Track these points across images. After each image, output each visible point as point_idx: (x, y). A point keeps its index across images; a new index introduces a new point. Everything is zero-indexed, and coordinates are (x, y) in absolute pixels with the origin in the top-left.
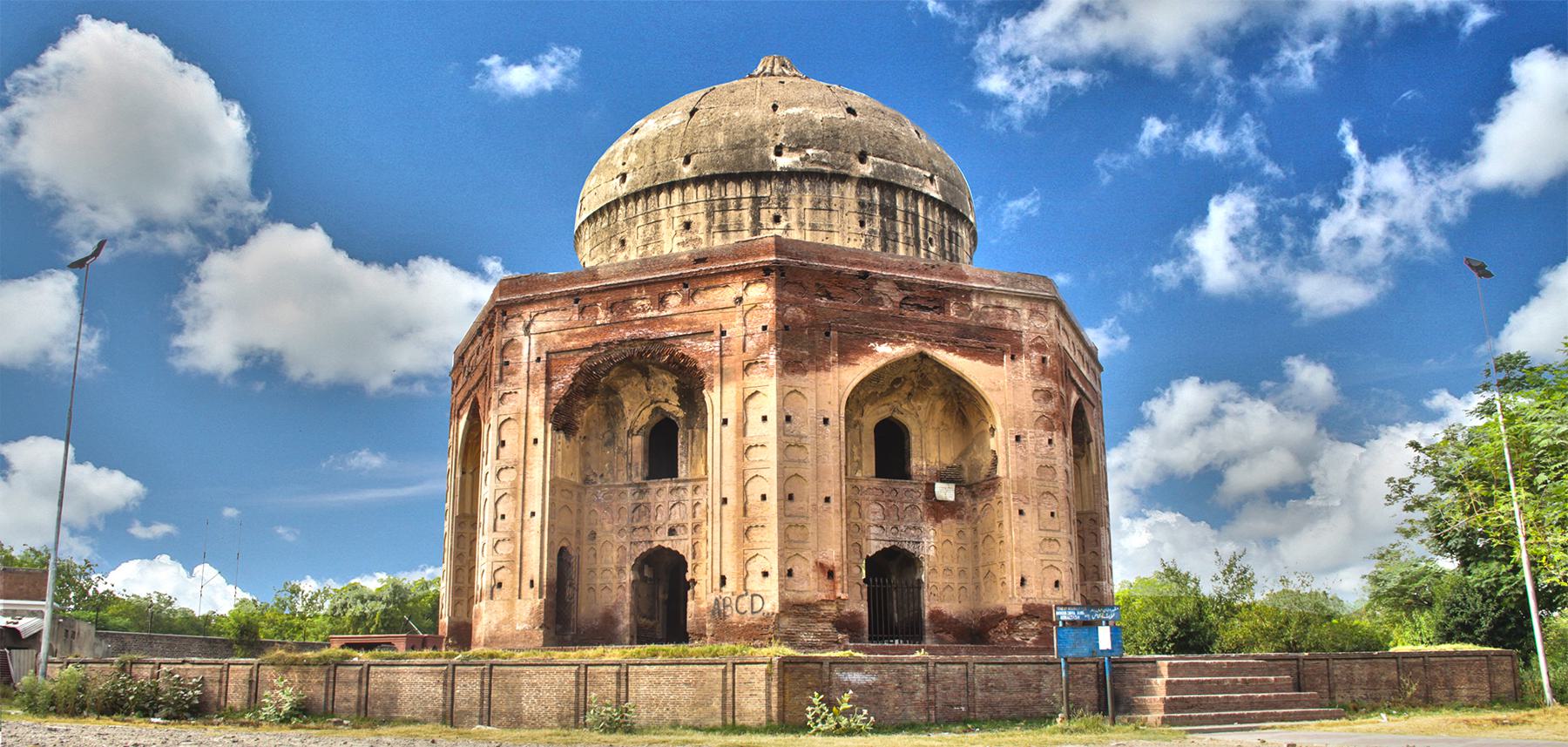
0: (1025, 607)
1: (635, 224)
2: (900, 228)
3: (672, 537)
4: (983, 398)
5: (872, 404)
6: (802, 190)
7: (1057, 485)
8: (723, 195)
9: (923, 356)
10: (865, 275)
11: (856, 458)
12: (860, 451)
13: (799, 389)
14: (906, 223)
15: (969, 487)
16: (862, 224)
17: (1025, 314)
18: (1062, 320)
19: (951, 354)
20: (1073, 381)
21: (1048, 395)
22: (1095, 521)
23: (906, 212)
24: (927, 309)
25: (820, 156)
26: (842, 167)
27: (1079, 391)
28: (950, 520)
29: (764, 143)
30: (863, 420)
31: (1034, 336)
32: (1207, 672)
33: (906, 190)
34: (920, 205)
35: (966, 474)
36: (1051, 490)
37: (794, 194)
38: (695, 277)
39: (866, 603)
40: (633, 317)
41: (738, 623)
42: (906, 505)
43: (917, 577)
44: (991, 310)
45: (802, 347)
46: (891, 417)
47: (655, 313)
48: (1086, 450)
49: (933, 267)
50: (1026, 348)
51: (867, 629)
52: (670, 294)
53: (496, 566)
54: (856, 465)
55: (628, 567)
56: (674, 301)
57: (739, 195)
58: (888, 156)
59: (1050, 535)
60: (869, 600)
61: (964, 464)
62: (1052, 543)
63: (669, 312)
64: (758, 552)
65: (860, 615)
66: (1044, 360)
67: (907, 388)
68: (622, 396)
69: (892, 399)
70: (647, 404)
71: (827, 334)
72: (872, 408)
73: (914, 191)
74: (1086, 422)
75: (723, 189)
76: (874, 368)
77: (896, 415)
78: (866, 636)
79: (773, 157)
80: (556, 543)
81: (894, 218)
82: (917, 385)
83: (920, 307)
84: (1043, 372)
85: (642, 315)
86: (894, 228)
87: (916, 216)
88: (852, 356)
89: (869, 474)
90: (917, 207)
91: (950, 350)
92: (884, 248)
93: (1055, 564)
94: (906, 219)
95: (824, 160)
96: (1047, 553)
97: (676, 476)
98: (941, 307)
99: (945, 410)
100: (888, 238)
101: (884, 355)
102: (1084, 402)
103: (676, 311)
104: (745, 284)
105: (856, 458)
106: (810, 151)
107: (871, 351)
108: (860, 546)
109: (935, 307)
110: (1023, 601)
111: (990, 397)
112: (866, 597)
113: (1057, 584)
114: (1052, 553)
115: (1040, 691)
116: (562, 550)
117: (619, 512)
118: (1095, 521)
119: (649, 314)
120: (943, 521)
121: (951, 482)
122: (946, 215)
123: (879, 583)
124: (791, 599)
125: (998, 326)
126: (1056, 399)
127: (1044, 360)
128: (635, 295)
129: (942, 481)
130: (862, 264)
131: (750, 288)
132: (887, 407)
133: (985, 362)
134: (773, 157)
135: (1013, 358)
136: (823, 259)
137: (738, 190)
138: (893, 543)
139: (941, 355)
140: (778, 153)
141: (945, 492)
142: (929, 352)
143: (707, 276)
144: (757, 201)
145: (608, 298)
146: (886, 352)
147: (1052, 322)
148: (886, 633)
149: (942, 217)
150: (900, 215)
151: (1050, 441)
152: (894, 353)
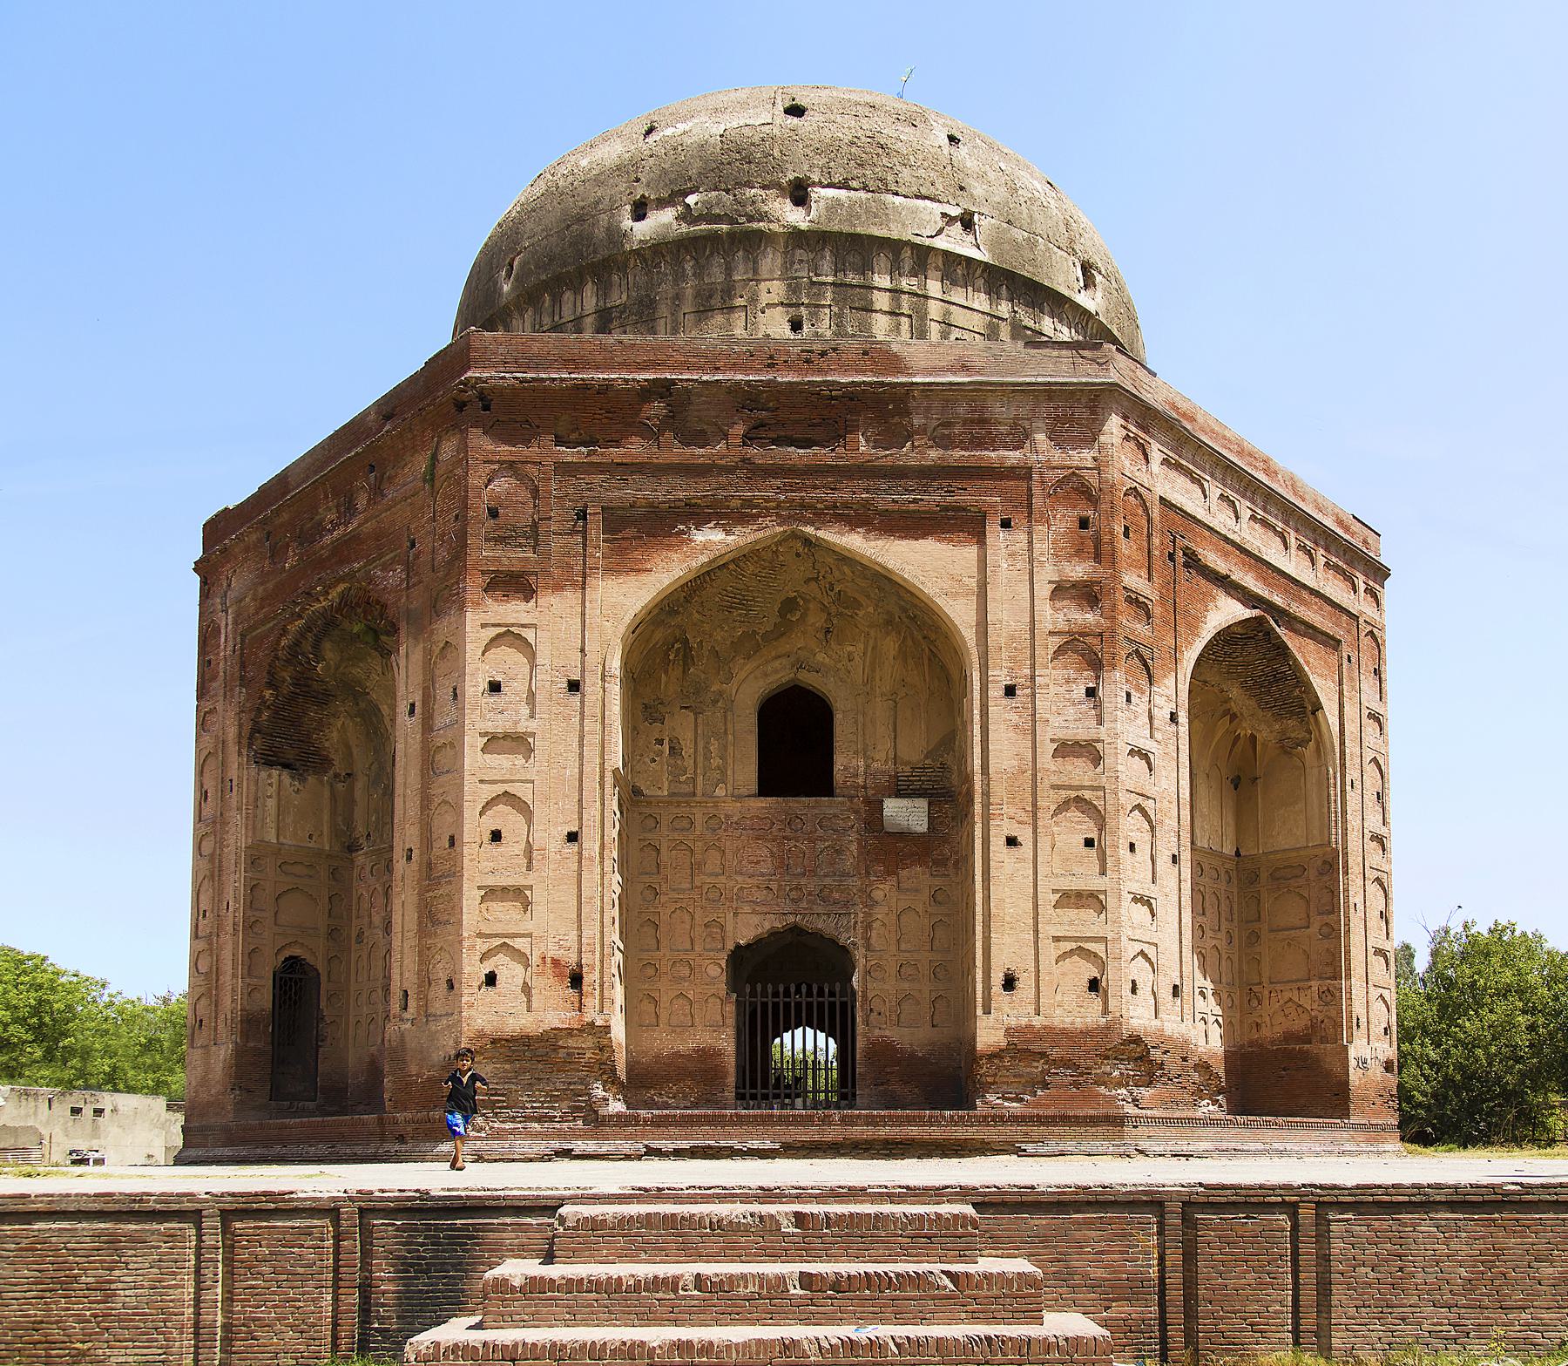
6: (680, 277)
8: (557, 318)
9: (795, 535)
11: (716, 762)
25: (708, 205)
26: (751, 219)
28: (919, 869)
29: (613, 209)
30: (731, 688)
32: (716, 1243)
33: (894, 247)
41: (418, 1076)
42: (821, 846)
48: (1312, 727)
49: (823, 354)
51: (731, 1080)
53: (934, 995)
54: (716, 775)
58: (854, 184)
65: (718, 1053)
67: (816, 619)
69: (797, 642)
72: (749, 667)
73: (914, 246)
78: (730, 1094)
79: (627, 223)
82: (833, 610)
89: (744, 791)
95: (716, 211)
99: (903, 655)
101: (705, 546)
105: (716, 762)
106: (691, 200)
108: (722, 927)
111: (960, 614)
112: (731, 1021)
115: (109, 1295)
116: (293, 964)
117: (251, 890)
120: (904, 873)
121: (920, 796)
129: (899, 794)
132: (784, 661)
134: (627, 223)
138: (791, 919)
139: (831, 535)
140: (639, 216)
141: (905, 813)
146: (712, 540)
148: (753, 1086)
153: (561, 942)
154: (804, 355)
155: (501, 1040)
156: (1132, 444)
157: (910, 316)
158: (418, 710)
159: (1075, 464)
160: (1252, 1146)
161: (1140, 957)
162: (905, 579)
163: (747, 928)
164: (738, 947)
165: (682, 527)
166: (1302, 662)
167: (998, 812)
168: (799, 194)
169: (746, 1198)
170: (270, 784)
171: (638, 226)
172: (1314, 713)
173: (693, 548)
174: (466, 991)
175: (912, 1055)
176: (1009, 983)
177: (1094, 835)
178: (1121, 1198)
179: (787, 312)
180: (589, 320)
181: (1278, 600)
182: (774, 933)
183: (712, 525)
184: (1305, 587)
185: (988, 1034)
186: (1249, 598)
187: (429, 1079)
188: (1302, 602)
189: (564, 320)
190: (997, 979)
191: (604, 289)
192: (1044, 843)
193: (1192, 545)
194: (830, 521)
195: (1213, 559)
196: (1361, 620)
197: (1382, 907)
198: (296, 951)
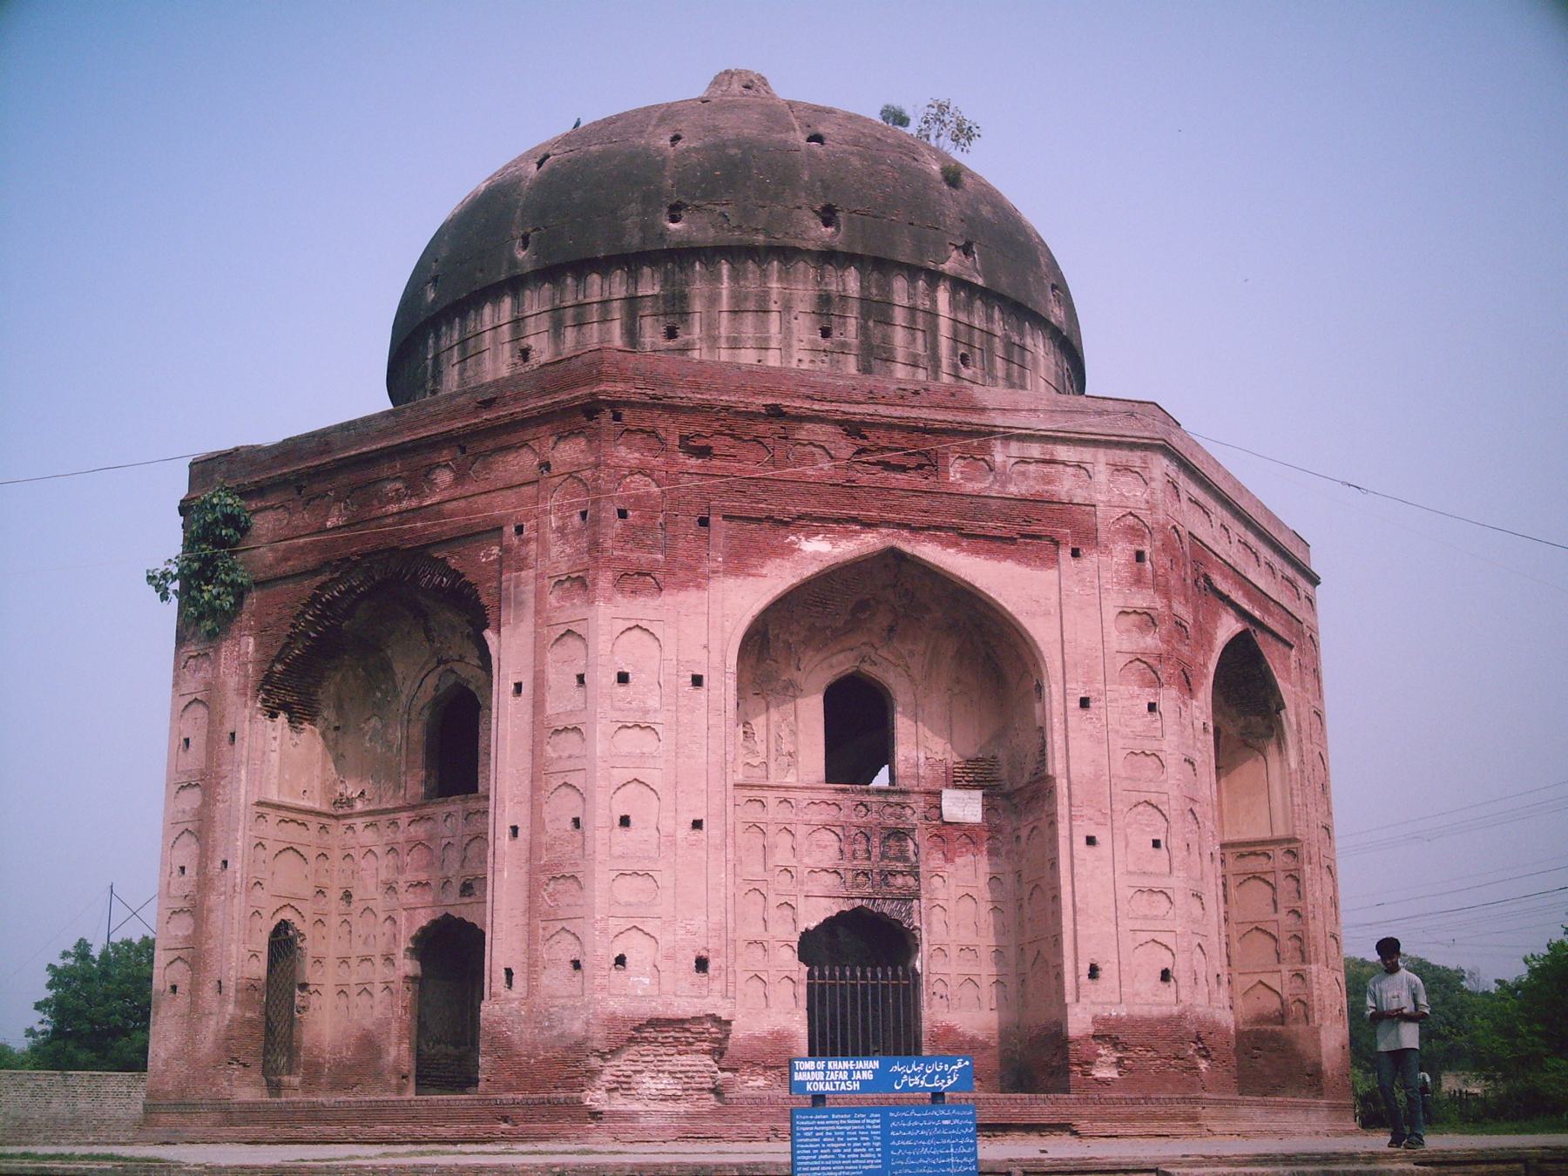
0: (1095, 1021)
1: (449, 360)
2: (899, 336)
3: (467, 900)
4: (1017, 630)
5: (818, 650)
7: (1166, 787)
10: (775, 413)
12: (794, 733)
13: (644, 624)
14: (911, 328)
15: (1007, 796)
16: (826, 333)
17: (1102, 474)
18: (1183, 481)
19: (951, 551)
20: (1225, 598)
21: (1149, 620)
22: (1295, 855)
23: (912, 309)
24: (904, 469)
27: (1243, 614)
31: (1119, 512)
34: (943, 297)
35: (1003, 773)
36: (1153, 798)
37: (698, 289)
38: (476, 433)
39: (804, 1013)
40: (379, 513)
41: (529, 1057)
43: (910, 965)
44: (1032, 468)
45: (651, 549)
46: (858, 672)
47: (414, 503)
49: (916, 393)
50: (1102, 536)
52: (438, 465)
55: (400, 953)
56: (444, 477)
57: (606, 295)
59: (1147, 882)
60: (810, 1009)
61: (1002, 755)
62: (1156, 897)
63: (437, 499)
64: (564, 924)
66: (1140, 556)
68: (389, 652)
70: (431, 666)
71: (704, 522)
74: (1268, 671)
75: (606, 287)
76: (794, 581)
77: (867, 668)
80: (266, 914)
81: (888, 322)
83: (887, 466)
84: (1138, 580)
85: (394, 508)
86: (887, 340)
87: (933, 314)
88: (754, 561)
90: (934, 301)
91: (947, 544)
92: (866, 369)
93: (1161, 938)
94: (913, 319)
96: (1145, 917)
97: (476, 790)
98: (930, 464)
100: (874, 354)
101: (816, 556)
102: (1260, 638)
103: (446, 495)
104: (554, 438)
107: (791, 550)
109: (920, 467)
110: (1098, 1010)
111: (1041, 631)
112: (803, 1003)
113: (1165, 975)
114: (1155, 918)
118: (1295, 855)
119: (405, 504)
121: (974, 788)
122: (997, 315)
123: (832, 976)
124: (620, 1011)
125: (1046, 497)
126: (1164, 628)
127: (1140, 556)
128: (386, 472)
130: (770, 391)
131: (561, 445)
133: (1019, 562)
135: (1075, 553)
136: (697, 387)
137: (606, 287)
138: (858, 902)
139: (930, 552)
142: (907, 548)
143: (494, 430)
144: (632, 302)
145: (344, 479)
147: (1158, 485)
149: (990, 319)
150: (899, 316)
151: (1152, 707)
152: (837, 551)
153: (688, 927)
154: (901, 392)
155: (266, 1013)
156: (1171, 485)
157: (924, 331)
158: (526, 689)
159: (1132, 505)
160: (1130, 1132)
161: (186, 834)
162: (991, 598)
163: (814, 914)
164: (802, 933)
165: (793, 538)
166: (1272, 668)
167: (1079, 813)
168: (828, 216)
169: (1318, 1162)
170: (275, 738)
171: (672, 226)
172: (1278, 712)
173: (803, 558)
174: (599, 973)
175: (973, 1039)
176: (1094, 972)
177: (1161, 837)
178: (1456, 1159)
179: (819, 321)
180: (616, 304)
181: (1257, 614)
182: (841, 914)
183: (820, 537)
184: (1270, 598)
185: (1079, 1022)
186: (1243, 614)
187: (546, 1060)
188: (1271, 614)
189: (587, 300)
190: (1084, 969)
191: (634, 277)
192: (1120, 844)
193: (1207, 571)
194: (924, 541)
195: (1223, 586)
196: (1305, 626)
197: (1331, 894)
198: (287, 915)
